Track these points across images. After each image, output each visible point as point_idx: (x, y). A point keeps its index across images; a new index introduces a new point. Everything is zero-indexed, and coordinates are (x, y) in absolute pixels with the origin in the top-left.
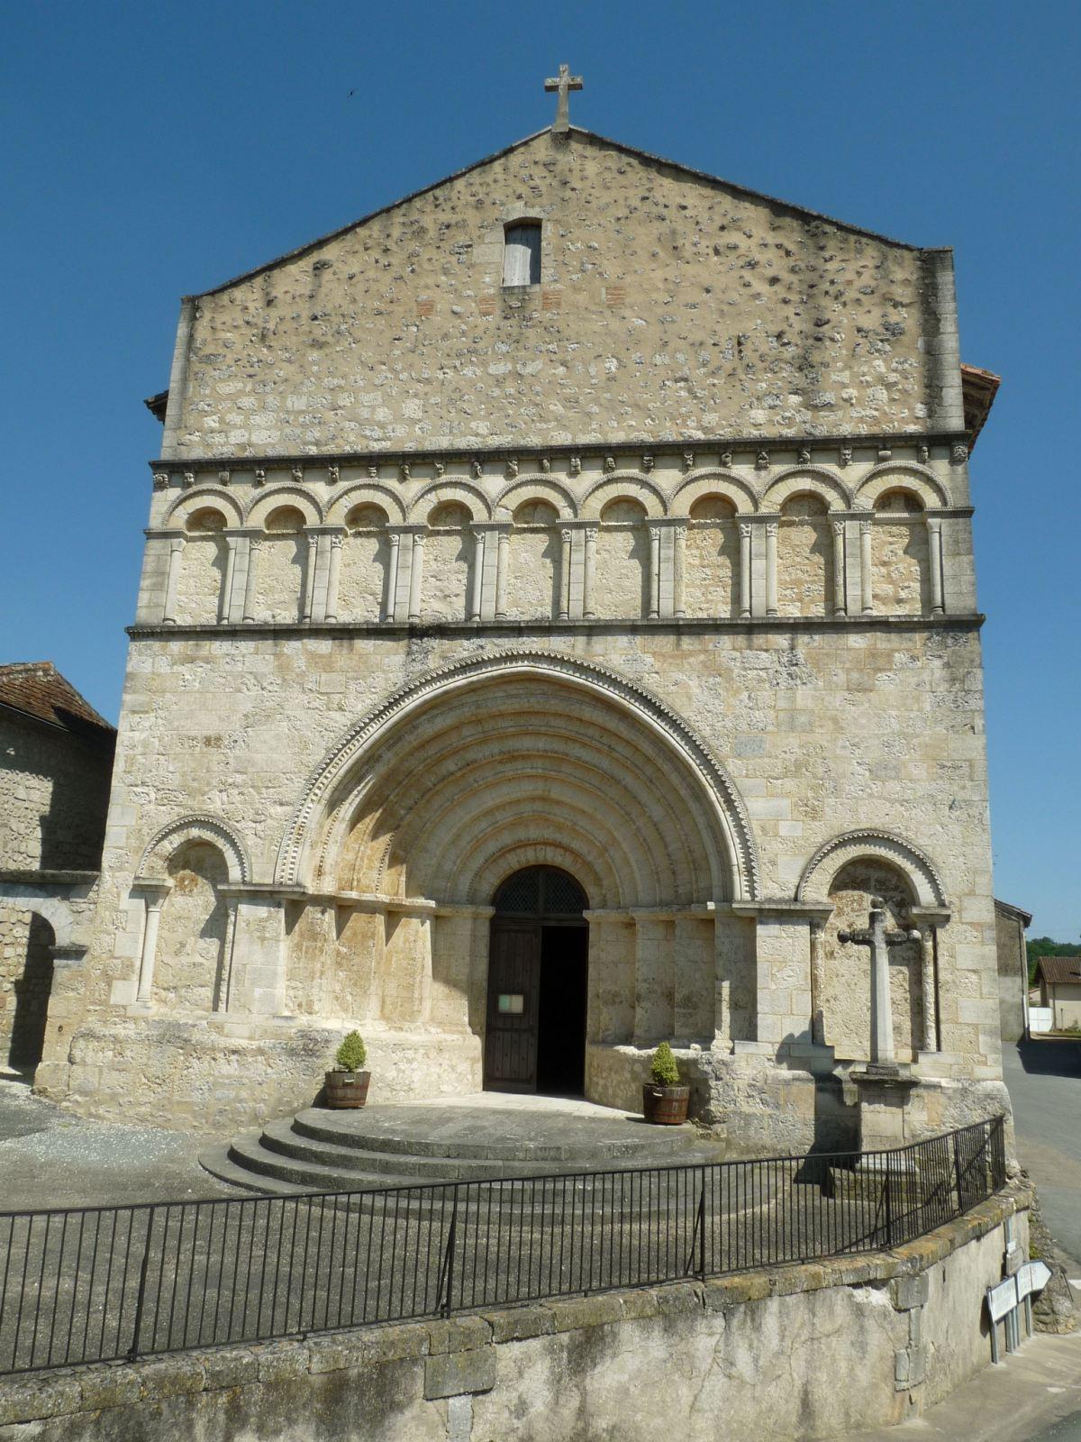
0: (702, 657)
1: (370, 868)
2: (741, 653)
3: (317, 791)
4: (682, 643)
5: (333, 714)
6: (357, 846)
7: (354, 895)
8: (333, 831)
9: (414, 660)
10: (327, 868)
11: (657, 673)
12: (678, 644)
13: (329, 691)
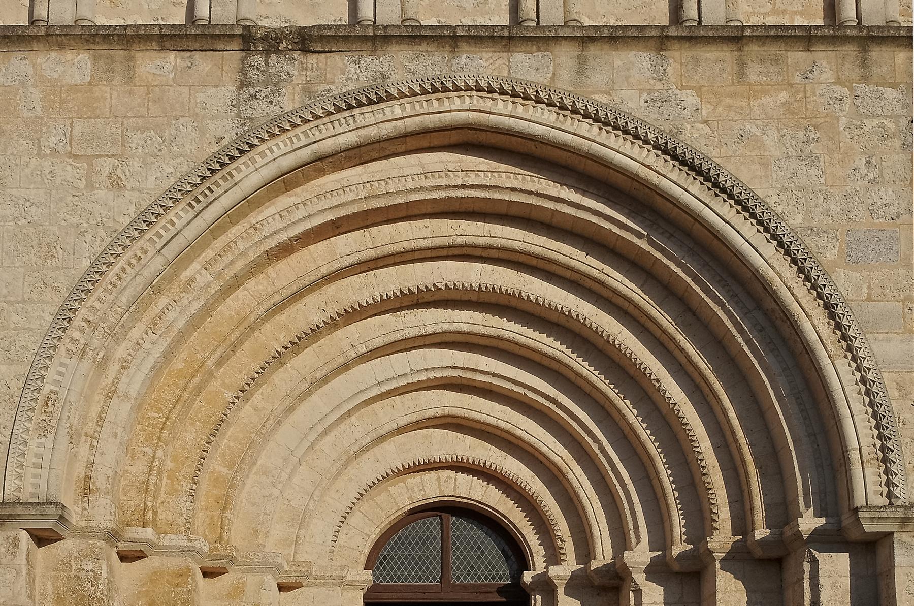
0: (784, 96)
1: (173, 492)
2: (851, 89)
3: (76, 335)
4: (748, 71)
5: (101, 194)
6: (150, 451)
7: (148, 533)
8: (110, 416)
9: (254, 97)
10: (100, 481)
11: (706, 122)
12: (741, 73)
13: (89, 152)
